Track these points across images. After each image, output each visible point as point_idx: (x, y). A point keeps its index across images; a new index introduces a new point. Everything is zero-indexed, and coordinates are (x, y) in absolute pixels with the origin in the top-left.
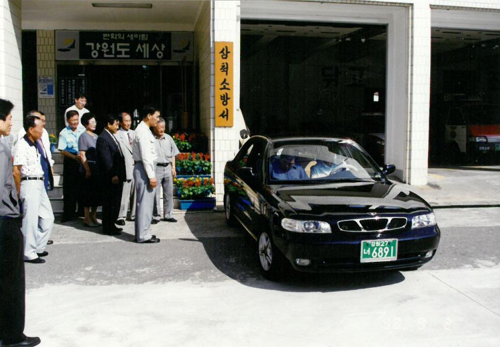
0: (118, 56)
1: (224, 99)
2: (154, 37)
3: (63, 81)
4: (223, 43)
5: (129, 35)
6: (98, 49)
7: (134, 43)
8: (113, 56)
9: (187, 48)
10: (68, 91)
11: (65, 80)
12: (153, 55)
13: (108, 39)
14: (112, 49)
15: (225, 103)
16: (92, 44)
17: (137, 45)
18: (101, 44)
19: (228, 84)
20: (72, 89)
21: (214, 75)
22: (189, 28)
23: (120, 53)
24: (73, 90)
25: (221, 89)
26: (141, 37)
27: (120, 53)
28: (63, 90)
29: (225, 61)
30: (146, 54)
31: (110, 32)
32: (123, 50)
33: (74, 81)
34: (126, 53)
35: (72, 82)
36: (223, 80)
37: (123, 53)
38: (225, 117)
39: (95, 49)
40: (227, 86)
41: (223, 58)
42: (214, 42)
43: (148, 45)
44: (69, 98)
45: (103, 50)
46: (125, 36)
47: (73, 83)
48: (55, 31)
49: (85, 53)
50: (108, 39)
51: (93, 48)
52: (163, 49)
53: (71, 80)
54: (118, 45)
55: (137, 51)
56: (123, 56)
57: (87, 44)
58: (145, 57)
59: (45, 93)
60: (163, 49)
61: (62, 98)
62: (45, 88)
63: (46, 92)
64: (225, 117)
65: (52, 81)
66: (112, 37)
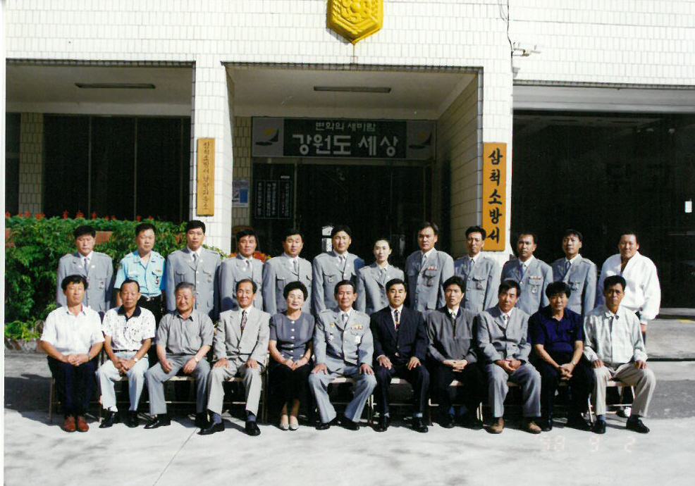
0: (335, 153)
1: (494, 216)
2: (385, 128)
3: (260, 184)
4: (494, 143)
5: (350, 125)
6: (308, 143)
7: (356, 136)
8: (328, 152)
9: (429, 142)
10: (266, 198)
11: (263, 183)
12: (381, 151)
13: (323, 130)
14: (326, 142)
15: (495, 220)
16: (301, 137)
17: (362, 138)
18: (312, 137)
19: (499, 197)
20: (272, 195)
21: (482, 184)
22: (434, 115)
23: (338, 148)
24: (274, 197)
25: (491, 203)
26: (366, 127)
27: (338, 148)
28: (260, 197)
29: (496, 167)
30: (373, 151)
31: (324, 121)
32: (342, 145)
33: (274, 185)
34: (346, 148)
35: (272, 186)
36: (493, 192)
37: (342, 148)
38: (495, 239)
39: (305, 142)
40: (498, 199)
41: (494, 164)
42: (482, 143)
43: (375, 138)
44: (268, 208)
45: (315, 145)
46: (344, 126)
47: (274, 188)
48: (252, 117)
49: (291, 148)
50: (323, 130)
51: (302, 141)
52: (395, 144)
53: (271, 183)
54: (336, 137)
55: (360, 145)
56: (342, 152)
57: (294, 136)
58: (370, 154)
59: (237, 201)
60: (395, 144)
61: (258, 207)
62: (237, 193)
63: (239, 199)
64: (495, 239)
65: (246, 184)
66: (328, 127)
